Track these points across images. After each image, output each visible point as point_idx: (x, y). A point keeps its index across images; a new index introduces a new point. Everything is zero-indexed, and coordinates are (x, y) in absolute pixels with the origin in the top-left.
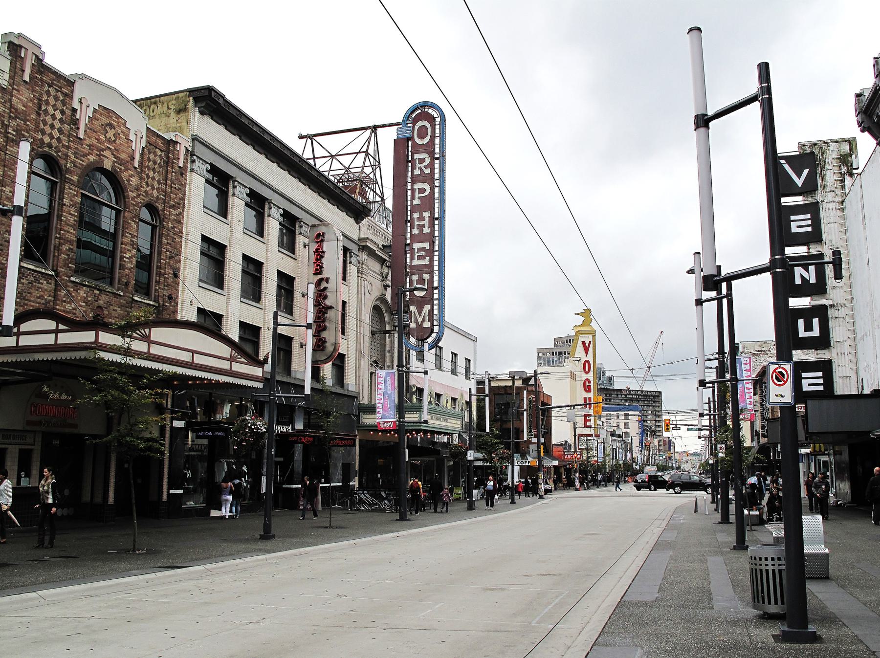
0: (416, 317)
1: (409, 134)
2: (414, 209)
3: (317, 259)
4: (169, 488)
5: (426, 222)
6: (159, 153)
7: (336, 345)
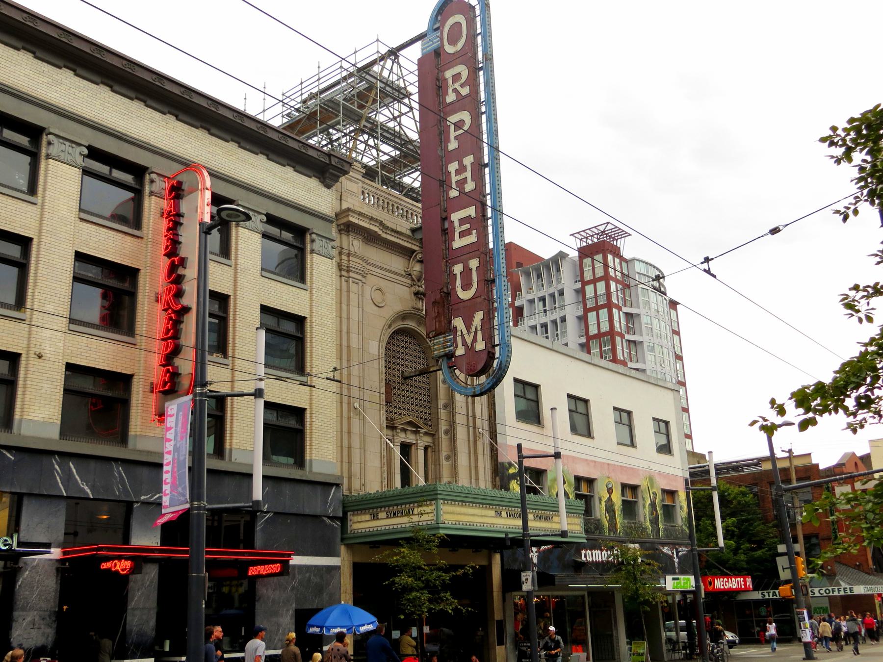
0: (466, 334)
3: (169, 229)
5: (468, 174)
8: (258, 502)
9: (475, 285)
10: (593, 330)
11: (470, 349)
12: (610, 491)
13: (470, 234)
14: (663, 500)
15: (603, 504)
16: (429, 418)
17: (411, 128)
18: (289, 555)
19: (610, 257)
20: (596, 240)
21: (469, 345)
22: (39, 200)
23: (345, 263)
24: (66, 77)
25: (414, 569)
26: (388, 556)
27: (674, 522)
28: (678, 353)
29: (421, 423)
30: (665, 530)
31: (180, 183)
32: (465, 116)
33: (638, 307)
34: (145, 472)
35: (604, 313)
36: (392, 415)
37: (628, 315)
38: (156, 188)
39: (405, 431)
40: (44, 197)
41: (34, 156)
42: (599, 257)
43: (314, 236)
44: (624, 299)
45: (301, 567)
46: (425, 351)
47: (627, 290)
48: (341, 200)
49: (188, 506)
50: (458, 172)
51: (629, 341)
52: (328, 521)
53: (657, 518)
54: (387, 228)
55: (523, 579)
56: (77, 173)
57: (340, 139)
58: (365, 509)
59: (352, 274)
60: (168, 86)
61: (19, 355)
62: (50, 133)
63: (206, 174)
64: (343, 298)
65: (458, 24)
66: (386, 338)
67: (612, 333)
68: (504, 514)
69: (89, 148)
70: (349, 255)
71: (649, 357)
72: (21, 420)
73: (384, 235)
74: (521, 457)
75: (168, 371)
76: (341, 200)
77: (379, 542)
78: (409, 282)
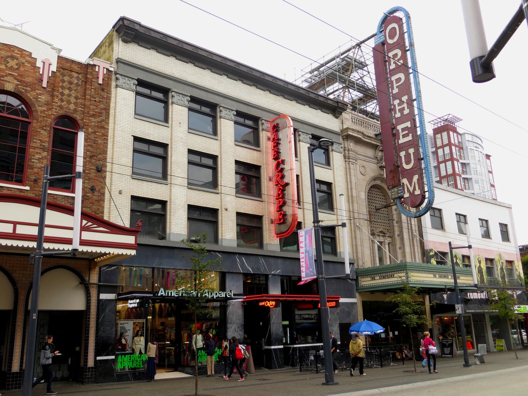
0: (409, 186)
1: (383, 39)
2: (395, 97)
3: (274, 147)
4: (97, 354)
5: (405, 105)
6: (75, 75)
7: (294, 216)
8: (348, 274)
9: (413, 162)
10: (443, 173)
11: (412, 194)
12: (480, 262)
13: (408, 136)
14: (506, 266)
15: (477, 269)
16: (389, 228)
17: (370, 81)
18: (339, 298)
19: (451, 133)
20: (442, 124)
21: (412, 192)
22: (170, 125)
23: (347, 154)
24: (224, 79)
25: (407, 304)
26: (393, 298)
27: (493, 276)
28: (492, 183)
29: (386, 232)
30: (509, 281)
31: (278, 124)
32: (402, 76)
33: (469, 159)
34: (339, 266)
35: (449, 164)
36: (373, 228)
37: (463, 165)
38: (265, 127)
39: (379, 235)
40: (221, 136)
41: (166, 103)
42: (445, 134)
43: (300, 133)
44: (460, 156)
45: (343, 303)
46: (385, 194)
47: (461, 151)
48: (342, 123)
49: (315, 277)
50: (399, 105)
51: (464, 178)
52: (350, 281)
53: (504, 275)
54: (365, 135)
55: (456, 308)
56: (132, 95)
57: (334, 91)
58: (368, 275)
59: (351, 160)
60: (200, 52)
61: (166, 201)
62: (173, 91)
63: (290, 119)
64: (348, 172)
65: (394, 28)
66: (367, 190)
67: (454, 174)
68: (437, 276)
69: (237, 111)
70: (348, 150)
71: (476, 186)
72: (170, 234)
73: (364, 139)
74: (451, 248)
75: (281, 214)
76: (342, 123)
77: (373, 291)
78: (376, 161)
